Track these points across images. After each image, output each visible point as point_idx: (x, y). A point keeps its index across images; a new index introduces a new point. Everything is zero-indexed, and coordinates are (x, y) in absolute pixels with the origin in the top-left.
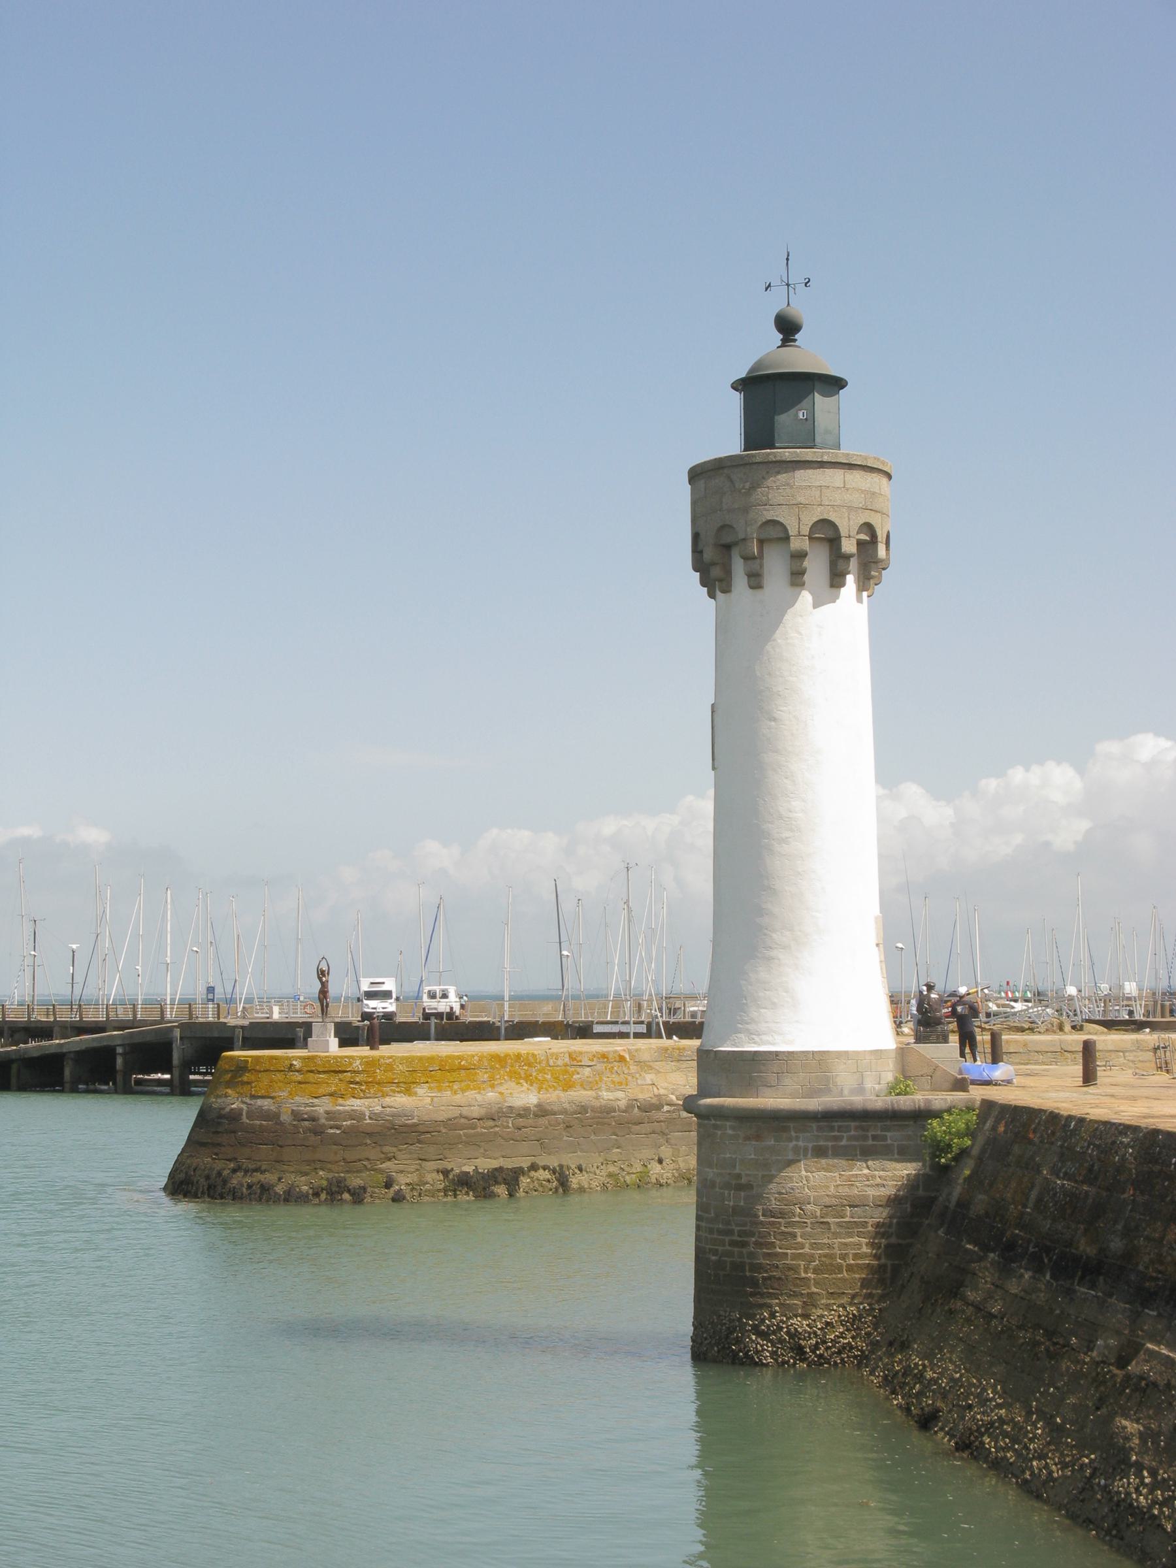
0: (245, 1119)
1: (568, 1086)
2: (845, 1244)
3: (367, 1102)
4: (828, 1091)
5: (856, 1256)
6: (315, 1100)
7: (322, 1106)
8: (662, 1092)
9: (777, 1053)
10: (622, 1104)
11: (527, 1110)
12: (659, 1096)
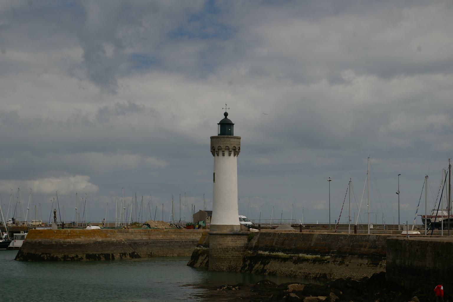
0: (43, 243)
1: (106, 237)
2: (374, 231)
3: (71, 240)
4: (233, 231)
5: (237, 255)
6: (60, 239)
7: (62, 241)
8: (122, 239)
9: (216, 225)
10: (115, 241)
11: (100, 242)
12: (121, 240)
